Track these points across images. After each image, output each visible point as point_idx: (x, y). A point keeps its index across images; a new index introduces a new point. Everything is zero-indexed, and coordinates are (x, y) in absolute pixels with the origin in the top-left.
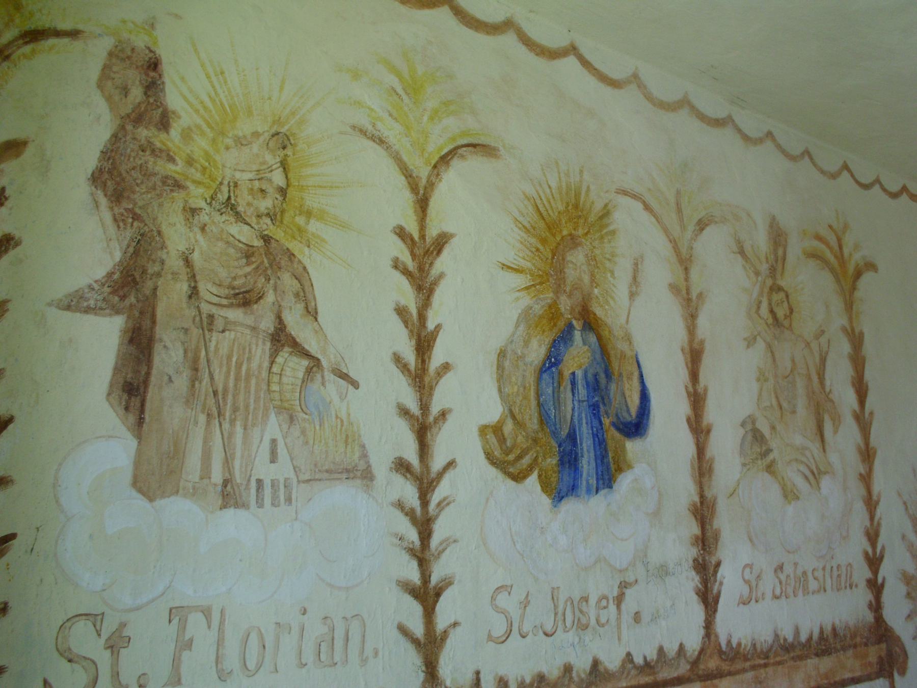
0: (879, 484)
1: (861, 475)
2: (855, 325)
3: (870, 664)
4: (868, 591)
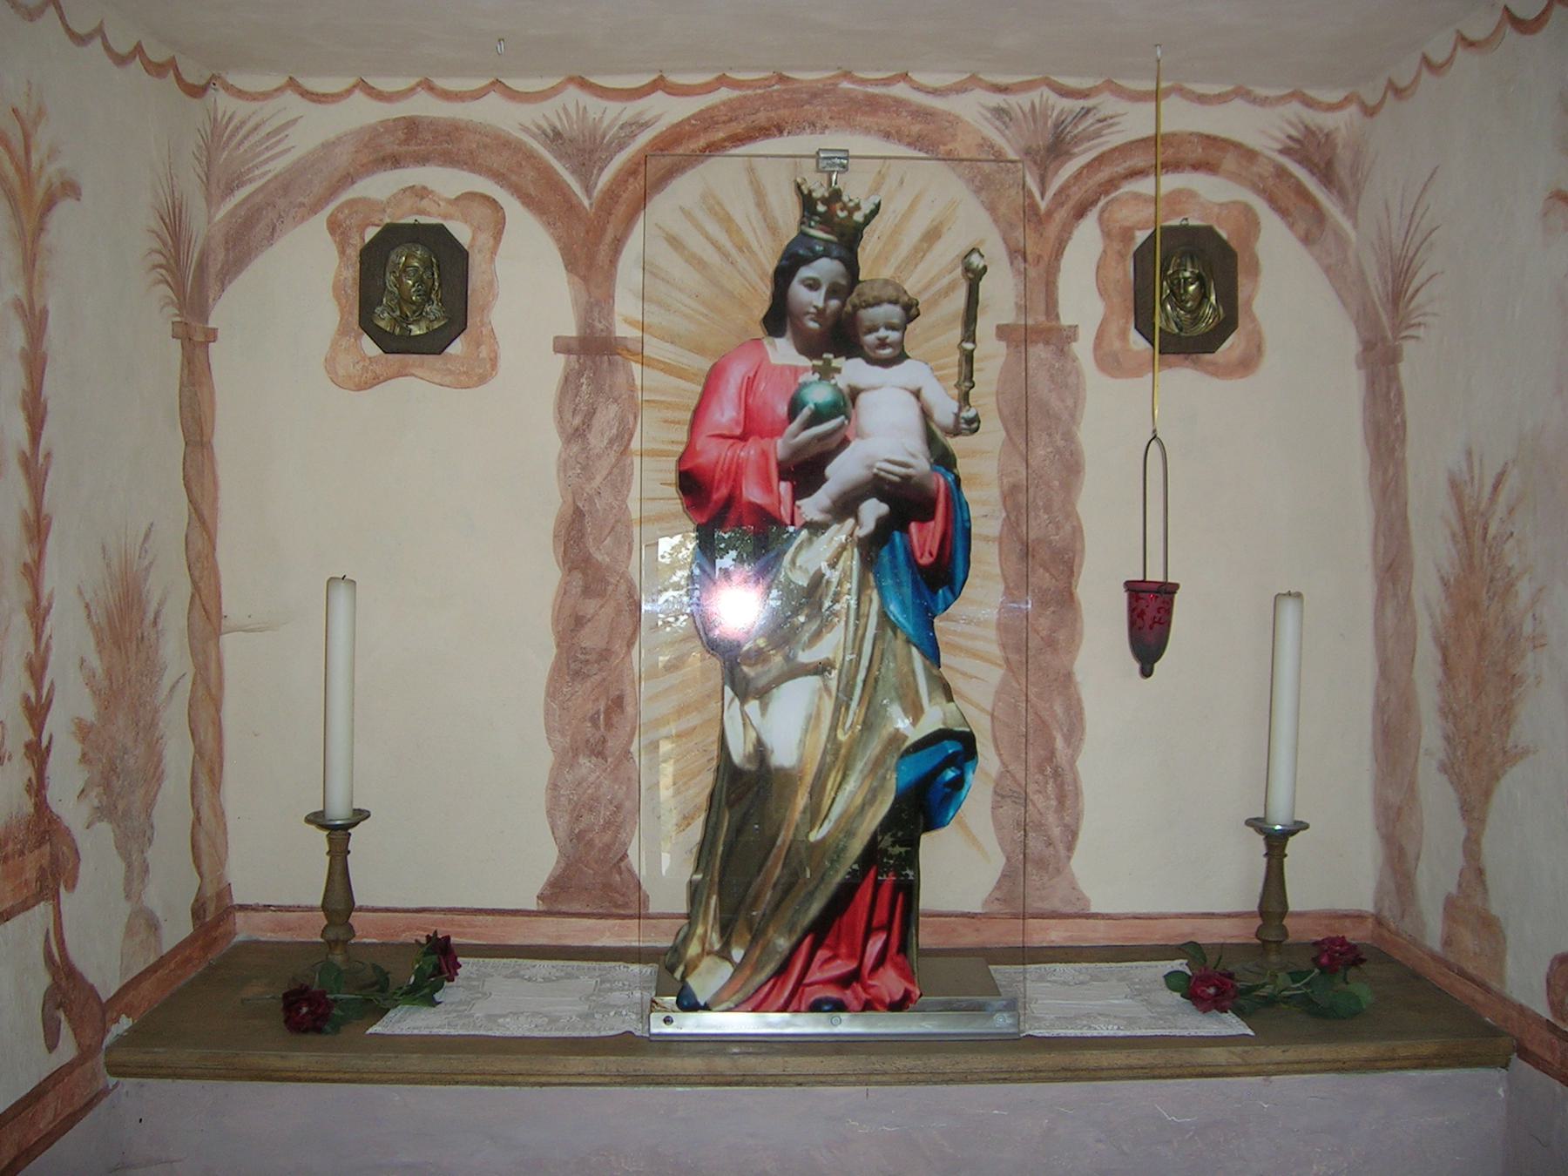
0: (53, 580)
1: (25, 565)
2: (35, 298)
3: (26, 883)
4: (27, 762)
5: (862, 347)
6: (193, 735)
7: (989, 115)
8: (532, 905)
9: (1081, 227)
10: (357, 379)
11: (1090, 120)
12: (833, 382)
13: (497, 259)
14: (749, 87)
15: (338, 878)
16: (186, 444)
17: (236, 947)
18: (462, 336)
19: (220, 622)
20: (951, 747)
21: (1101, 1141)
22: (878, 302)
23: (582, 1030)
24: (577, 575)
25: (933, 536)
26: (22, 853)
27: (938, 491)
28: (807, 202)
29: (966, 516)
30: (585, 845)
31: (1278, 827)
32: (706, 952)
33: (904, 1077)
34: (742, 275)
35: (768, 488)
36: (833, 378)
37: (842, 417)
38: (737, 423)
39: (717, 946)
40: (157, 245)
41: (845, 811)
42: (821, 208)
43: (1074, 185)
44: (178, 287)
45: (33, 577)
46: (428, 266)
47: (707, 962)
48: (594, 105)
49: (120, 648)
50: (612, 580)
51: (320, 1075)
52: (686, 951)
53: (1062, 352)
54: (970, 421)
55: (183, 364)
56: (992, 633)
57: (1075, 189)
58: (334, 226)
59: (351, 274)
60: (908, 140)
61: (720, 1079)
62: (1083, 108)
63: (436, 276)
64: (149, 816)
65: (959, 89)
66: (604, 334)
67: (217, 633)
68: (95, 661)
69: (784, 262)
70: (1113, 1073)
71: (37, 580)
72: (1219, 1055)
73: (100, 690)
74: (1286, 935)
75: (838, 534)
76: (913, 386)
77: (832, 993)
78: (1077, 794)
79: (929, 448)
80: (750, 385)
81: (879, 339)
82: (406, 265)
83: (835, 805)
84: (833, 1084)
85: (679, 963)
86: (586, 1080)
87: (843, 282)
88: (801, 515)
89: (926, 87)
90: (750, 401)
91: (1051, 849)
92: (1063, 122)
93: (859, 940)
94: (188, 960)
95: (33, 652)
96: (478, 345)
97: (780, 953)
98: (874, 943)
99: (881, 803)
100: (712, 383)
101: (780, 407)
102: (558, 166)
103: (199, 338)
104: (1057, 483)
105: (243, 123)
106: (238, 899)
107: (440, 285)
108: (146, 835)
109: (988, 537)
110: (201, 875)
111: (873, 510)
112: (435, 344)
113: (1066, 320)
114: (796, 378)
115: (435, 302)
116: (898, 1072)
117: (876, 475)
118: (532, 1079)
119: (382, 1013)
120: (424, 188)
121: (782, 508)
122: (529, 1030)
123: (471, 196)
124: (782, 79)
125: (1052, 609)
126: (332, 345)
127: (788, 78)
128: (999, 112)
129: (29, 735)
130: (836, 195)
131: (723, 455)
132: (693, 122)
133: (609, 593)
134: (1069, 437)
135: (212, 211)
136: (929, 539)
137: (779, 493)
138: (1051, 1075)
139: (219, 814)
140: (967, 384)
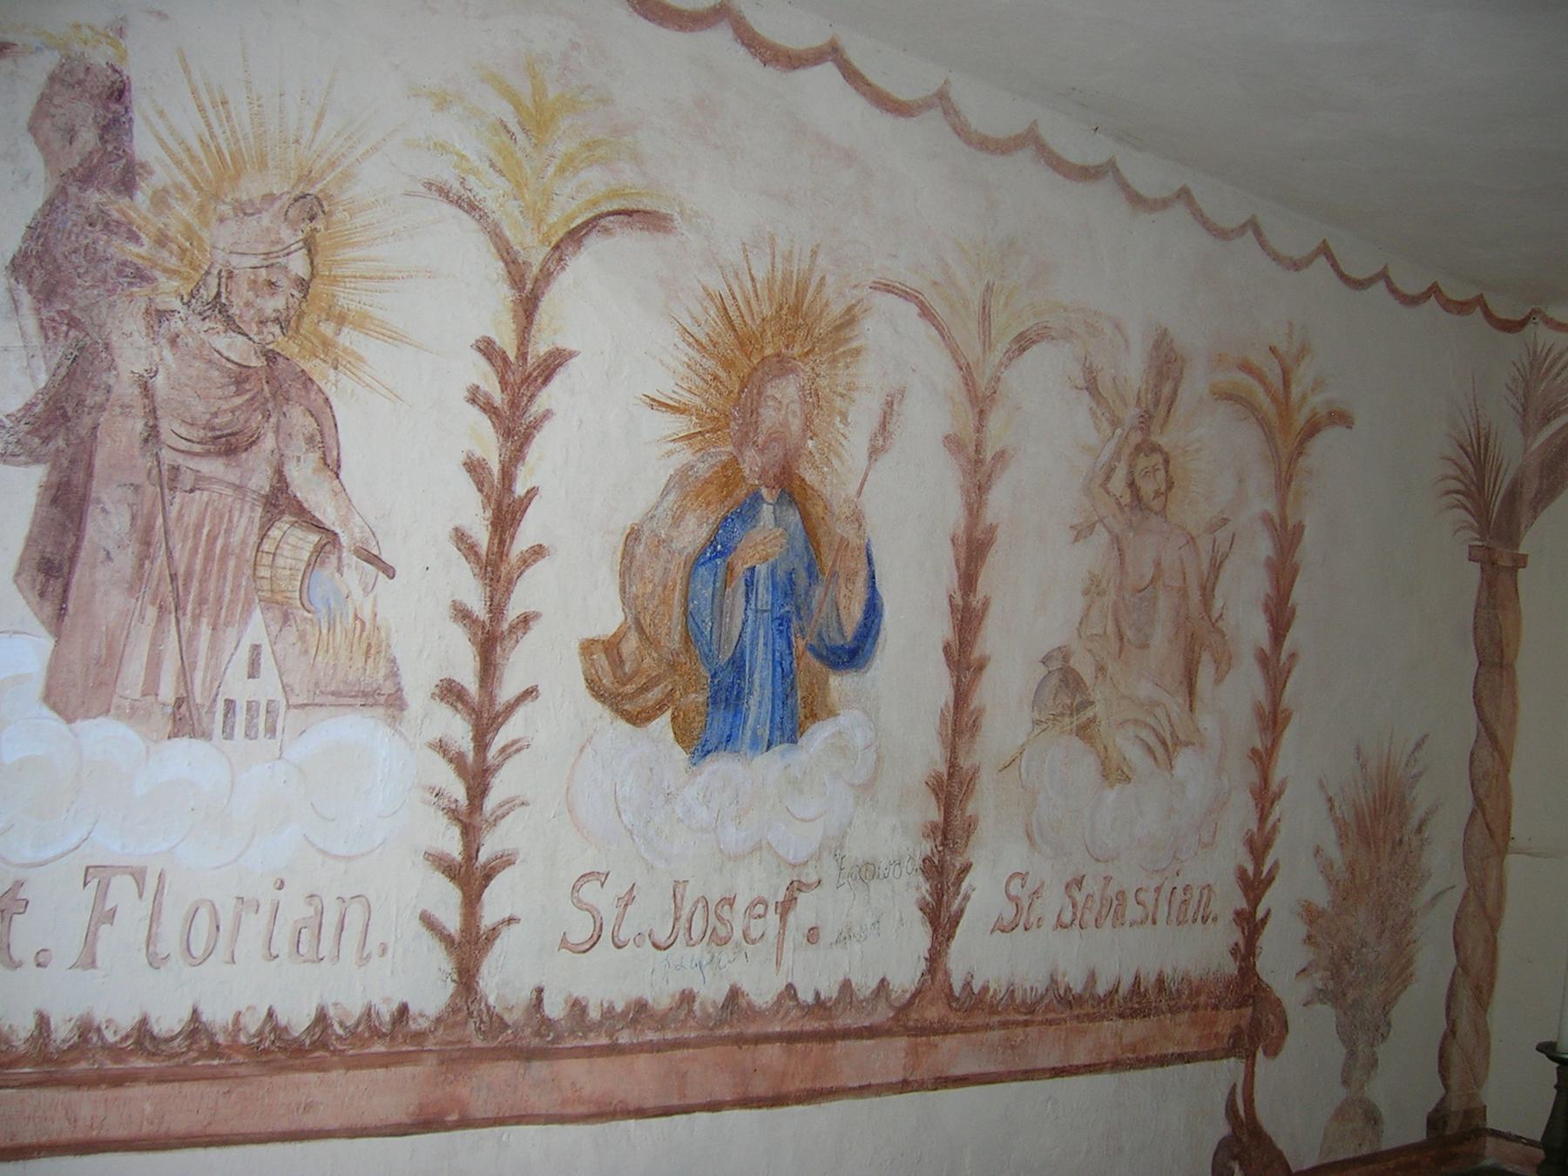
1: (1254, 751)
6: (1457, 947)
26: (1215, 1007)
40: (1452, 470)
44: (1481, 513)
45: (1261, 763)
49: (1369, 845)
55: (1481, 586)
64: (1386, 1014)
67: (1502, 852)
68: (1333, 852)
71: (1268, 767)
73: (1338, 881)
95: (1255, 830)
103: (1505, 562)
108: (1380, 1029)
110: (1446, 1086)
129: (1241, 903)
135: (1529, 441)
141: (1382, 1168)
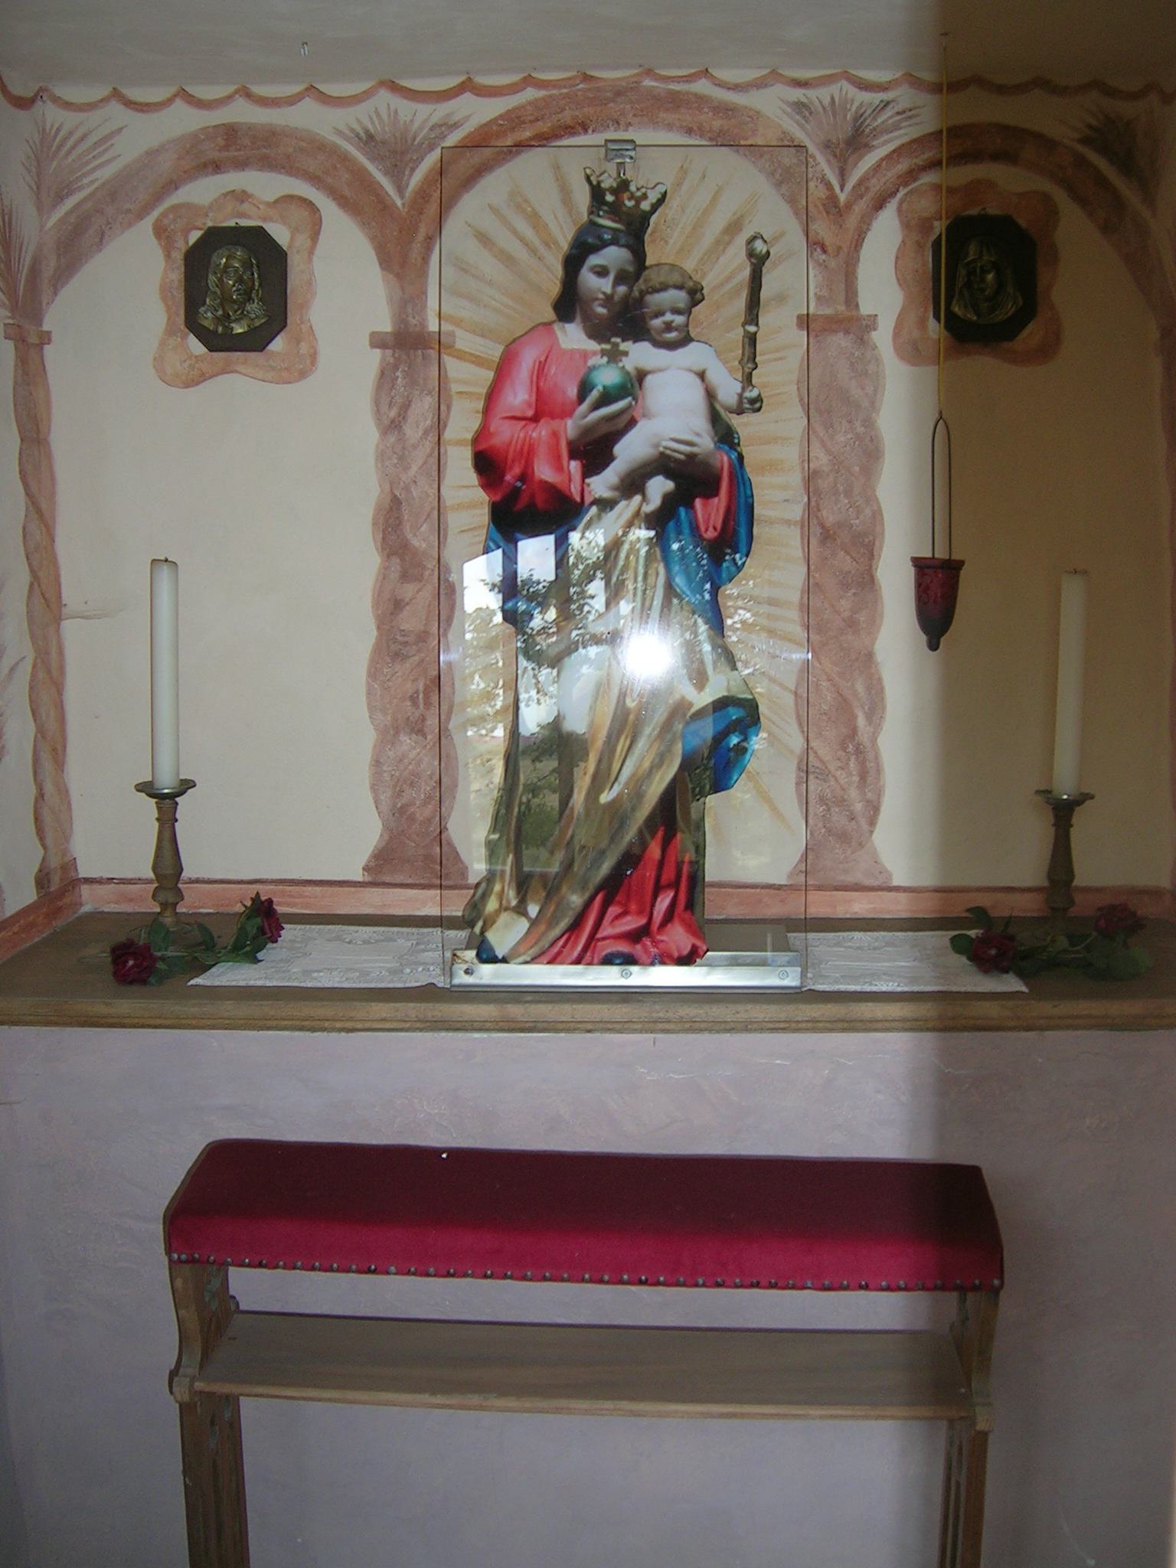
5: (648, 330)
6: (34, 713)
7: (789, 110)
8: (358, 876)
9: (880, 218)
10: (184, 377)
11: (888, 113)
12: (621, 365)
13: (315, 259)
14: (554, 87)
15: (167, 844)
16: (22, 440)
17: (80, 918)
18: (282, 334)
19: (60, 610)
20: (734, 713)
21: (879, 1092)
22: (664, 288)
23: (389, 982)
24: (396, 560)
25: (718, 510)
27: (722, 469)
28: (597, 193)
29: (749, 493)
30: (407, 819)
31: (1065, 797)
32: (503, 908)
33: (687, 1026)
34: (548, 269)
35: (559, 468)
36: (621, 361)
37: (630, 399)
38: (529, 405)
39: (514, 903)
41: (633, 775)
42: (609, 198)
43: (873, 176)
46: (247, 265)
47: (504, 917)
48: (406, 109)
50: (430, 566)
51: (142, 1021)
52: (484, 905)
53: (862, 341)
54: (752, 401)
55: (16, 365)
56: (794, 614)
57: (874, 181)
58: (160, 231)
59: (177, 276)
60: (709, 135)
61: (513, 1025)
62: (882, 101)
63: (256, 275)
65: (759, 84)
66: (417, 329)
67: (58, 619)
69: (574, 251)
70: (887, 1025)
72: (992, 1010)
74: (1072, 903)
75: (626, 508)
76: (698, 368)
77: (623, 948)
78: (879, 770)
79: (713, 427)
80: (541, 369)
81: (665, 323)
82: (227, 266)
83: (625, 768)
84: (620, 1032)
85: (480, 918)
86: (387, 1025)
87: (631, 269)
88: (590, 492)
89: (726, 83)
90: (542, 384)
91: (854, 822)
92: (862, 115)
93: (648, 899)
94: (31, 926)
96: (298, 342)
97: (573, 909)
98: (662, 900)
99: (668, 767)
100: (503, 370)
101: (569, 389)
102: (371, 168)
103: (33, 339)
104: (857, 469)
105: (71, 133)
106: (83, 873)
107: (260, 285)
109: (790, 520)
111: (659, 487)
112: (256, 341)
113: (866, 308)
114: (585, 362)
115: (256, 301)
116: (681, 1020)
117: (662, 454)
118: (338, 1025)
119: (206, 968)
120: (244, 192)
121: (572, 486)
122: (339, 982)
123: (290, 198)
124: (587, 78)
125: (853, 591)
126: (160, 345)
127: (592, 77)
128: (800, 107)
130: (623, 185)
131: (516, 436)
132: (501, 122)
133: (426, 578)
134: (869, 423)
136: (713, 515)
137: (570, 472)
138: (828, 1025)
139: (64, 792)
140: (750, 365)
141: (10, 934)
